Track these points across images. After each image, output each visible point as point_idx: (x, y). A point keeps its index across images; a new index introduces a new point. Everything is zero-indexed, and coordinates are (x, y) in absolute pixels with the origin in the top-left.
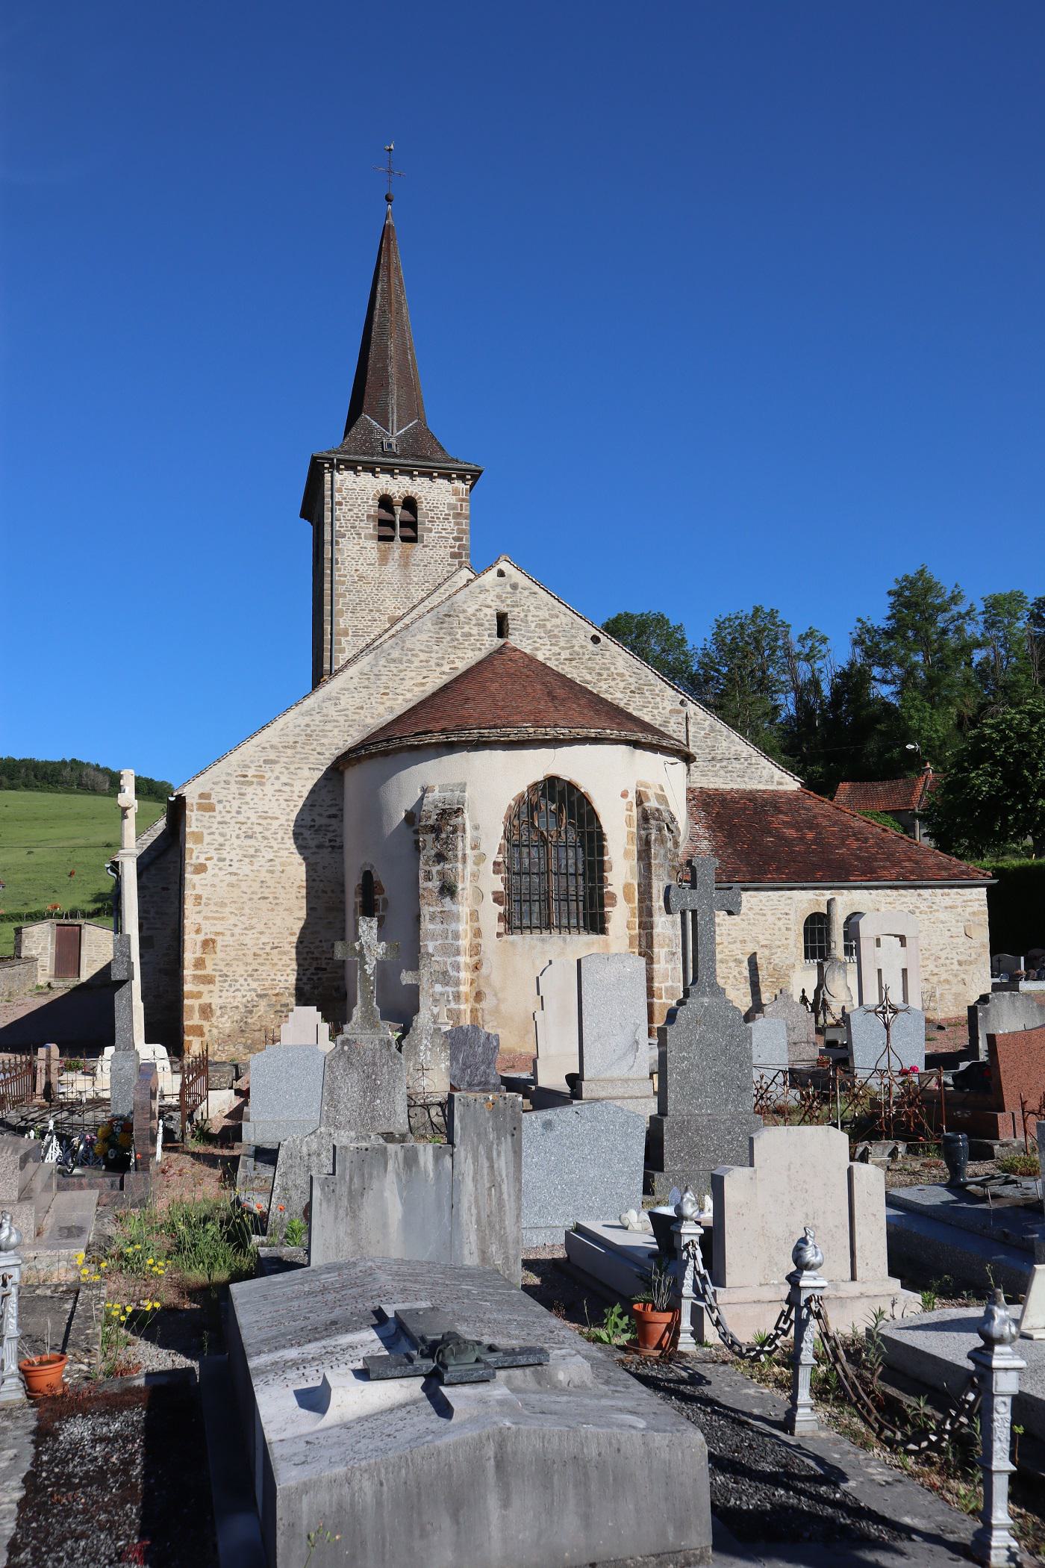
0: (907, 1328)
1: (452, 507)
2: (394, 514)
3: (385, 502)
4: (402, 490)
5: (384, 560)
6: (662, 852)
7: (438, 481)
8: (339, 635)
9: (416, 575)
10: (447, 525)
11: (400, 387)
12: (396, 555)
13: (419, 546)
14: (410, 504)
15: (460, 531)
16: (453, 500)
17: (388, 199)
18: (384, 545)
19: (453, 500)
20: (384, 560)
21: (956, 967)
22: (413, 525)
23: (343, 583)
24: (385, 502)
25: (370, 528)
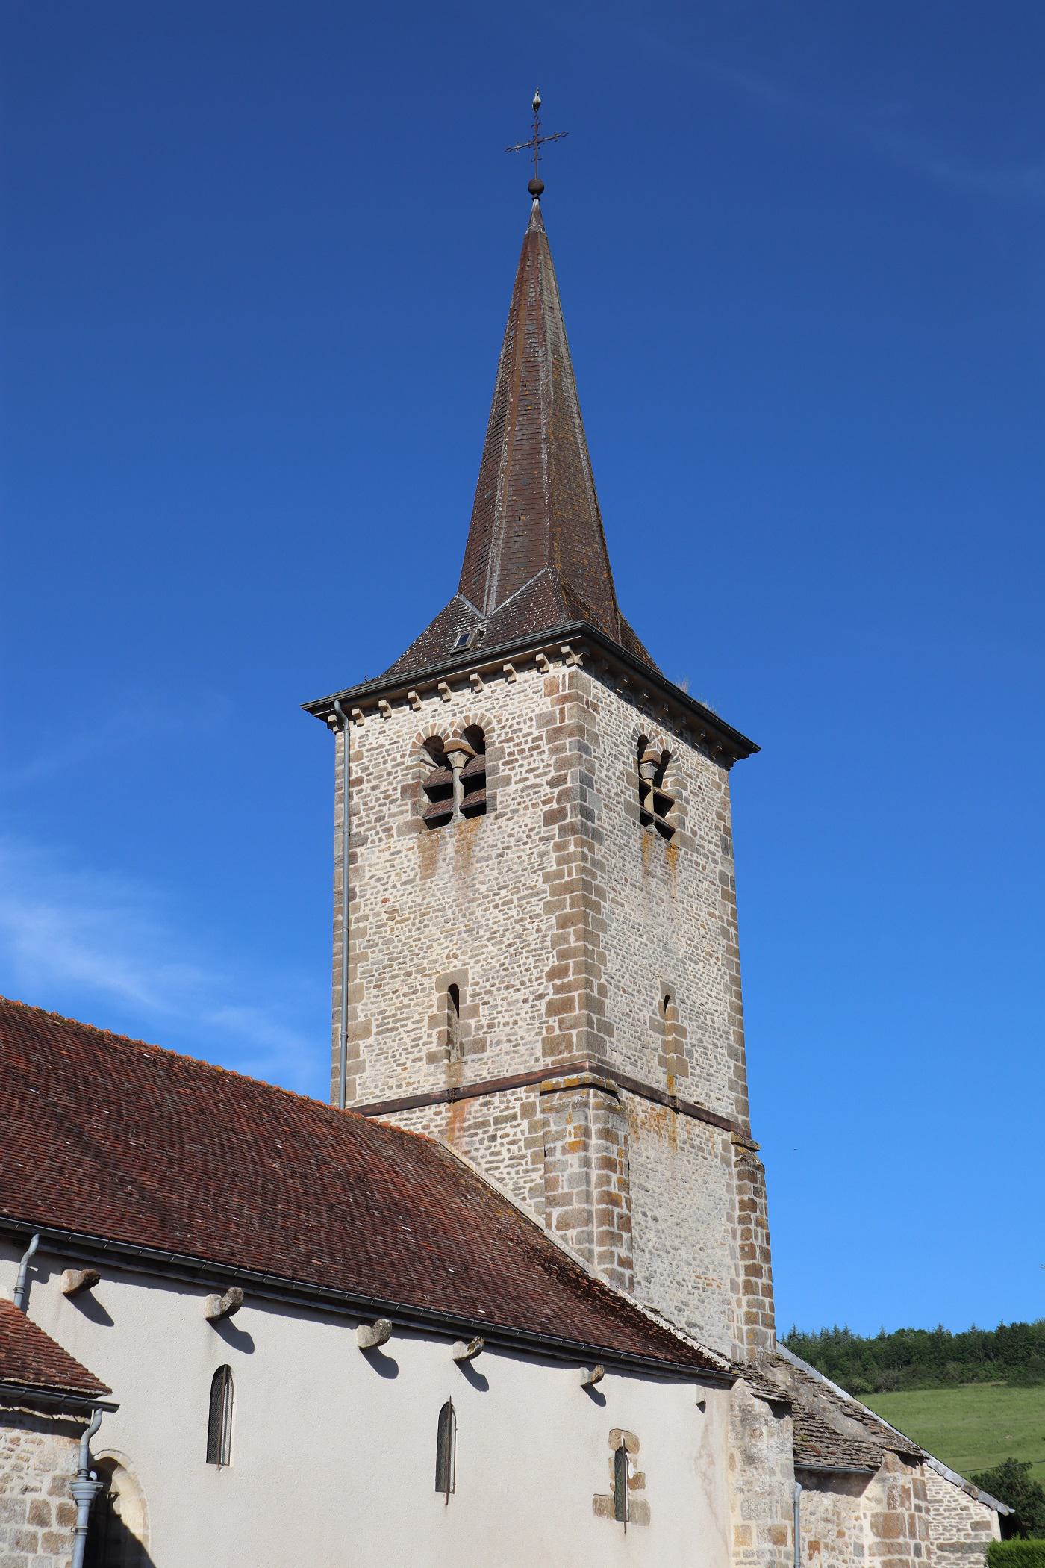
0: (713, 1513)
1: (545, 719)
2: (450, 768)
3: (435, 747)
4: (459, 719)
5: (429, 865)
8: (357, 1037)
9: (486, 875)
10: (537, 761)
12: (450, 850)
13: (488, 819)
14: (476, 736)
15: (561, 764)
17: (536, 192)
18: (429, 837)
20: (429, 865)
22: (475, 782)
23: (363, 933)
24: (435, 747)
25: (404, 813)
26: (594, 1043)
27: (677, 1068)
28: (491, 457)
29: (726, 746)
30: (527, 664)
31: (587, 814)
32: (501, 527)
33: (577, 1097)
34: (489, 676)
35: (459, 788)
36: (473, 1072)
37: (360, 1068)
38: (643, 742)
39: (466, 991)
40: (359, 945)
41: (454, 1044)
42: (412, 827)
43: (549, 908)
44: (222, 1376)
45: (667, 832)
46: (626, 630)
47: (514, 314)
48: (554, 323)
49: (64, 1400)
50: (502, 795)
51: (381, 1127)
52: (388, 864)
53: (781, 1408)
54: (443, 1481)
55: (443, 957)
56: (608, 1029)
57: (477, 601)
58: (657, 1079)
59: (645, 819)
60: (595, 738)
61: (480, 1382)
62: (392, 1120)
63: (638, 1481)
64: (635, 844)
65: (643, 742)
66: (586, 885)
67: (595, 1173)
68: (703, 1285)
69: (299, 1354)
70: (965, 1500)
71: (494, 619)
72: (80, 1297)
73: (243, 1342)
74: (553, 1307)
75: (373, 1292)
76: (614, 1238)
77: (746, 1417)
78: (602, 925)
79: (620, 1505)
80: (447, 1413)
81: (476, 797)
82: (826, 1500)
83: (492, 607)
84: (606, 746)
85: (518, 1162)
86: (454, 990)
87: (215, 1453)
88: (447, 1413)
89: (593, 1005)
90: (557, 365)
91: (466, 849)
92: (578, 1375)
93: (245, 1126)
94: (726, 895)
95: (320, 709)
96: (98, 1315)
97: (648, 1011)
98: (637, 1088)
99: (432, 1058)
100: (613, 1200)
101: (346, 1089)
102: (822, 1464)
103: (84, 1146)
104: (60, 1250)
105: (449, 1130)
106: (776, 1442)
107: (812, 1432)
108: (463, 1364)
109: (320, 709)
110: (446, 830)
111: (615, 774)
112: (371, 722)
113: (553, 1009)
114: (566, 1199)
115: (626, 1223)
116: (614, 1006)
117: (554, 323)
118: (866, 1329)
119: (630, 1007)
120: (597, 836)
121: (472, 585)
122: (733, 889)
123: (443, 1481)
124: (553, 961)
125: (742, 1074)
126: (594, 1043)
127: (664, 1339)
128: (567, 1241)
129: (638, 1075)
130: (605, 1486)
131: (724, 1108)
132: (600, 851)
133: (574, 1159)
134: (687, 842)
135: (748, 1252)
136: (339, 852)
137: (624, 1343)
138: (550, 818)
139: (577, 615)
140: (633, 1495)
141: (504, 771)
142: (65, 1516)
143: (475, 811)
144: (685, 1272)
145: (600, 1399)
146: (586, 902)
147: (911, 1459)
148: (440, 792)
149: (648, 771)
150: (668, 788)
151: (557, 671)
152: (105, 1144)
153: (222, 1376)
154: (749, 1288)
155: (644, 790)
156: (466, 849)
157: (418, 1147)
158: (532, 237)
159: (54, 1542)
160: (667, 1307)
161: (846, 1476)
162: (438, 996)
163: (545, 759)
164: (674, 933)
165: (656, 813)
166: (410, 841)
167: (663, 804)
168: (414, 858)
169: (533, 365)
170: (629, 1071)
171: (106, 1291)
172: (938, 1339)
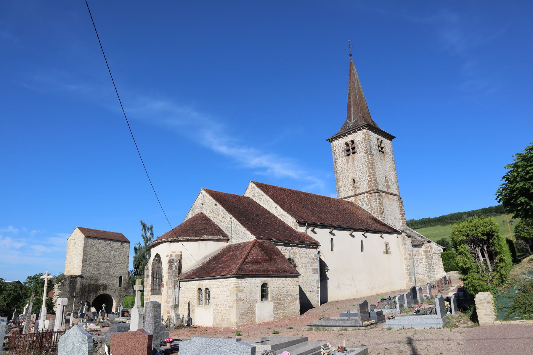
1: (363, 138)
3: (347, 144)
5: (348, 162)
6: (171, 271)
7: (353, 134)
9: (357, 163)
10: (362, 145)
11: (354, 107)
13: (356, 154)
14: (353, 142)
15: (366, 145)
16: (363, 136)
17: (351, 55)
19: (363, 136)
20: (348, 162)
21: (228, 308)
24: (347, 144)
25: (343, 154)
26: (376, 186)
27: (388, 188)
28: (349, 98)
29: (390, 137)
30: (359, 130)
31: (371, 152)
32: (352, 109)
33: (374, 194)
34: (354, 132)
35: (351, 150)
36: (358, 192)
37: (341, 192)
38: (378, 139)
39: (356, 180)
40: (339, 174)
41: (355, 188)
42: (344, 156)
43: (367, 167)
44: (332, 239)
45: (383, 152)
46: (373, 122)
47: (350, 75)
48: (356, 75)
49: (314, 245)
50: (357, 150)
51: (346, 201)
52: (341, 162)
53: (409, 237)
54: (362, 251)
55: (352, 175)
56: (378, 184)
57: (350, 121)
58: (385, 190)
59: (380, 151)
60: (371, 140)
61: (366, 237)
62: (347, 200)
63: (389, 249)
64: (379, 155)
65: (378, 139)
66: (372, 163)
67: (378, 205)
68: (395, 219)
69: (341, 235)
70: (437, 247)
71: (353, 123)
72: (313, 231)
73: (334, 235)
74: (374, 225)
75: (350, 226)
76: (382, 214)
77: (404, 238)
78: (375, 168)
79: (387, 252)
80: (362, 241)
81: (354, 151)
82: (416, 249)
83: (352, 121)
84: (373, 141)
85: (366, 204)
86: (354, 180)
87: (332, 250)
88: (362, 241)
89: (375, 180)
90: (358, 82)
91: (353, 159)
92: (379, 235)
93: (328, 204)
94: (393, 161)
95: (328, 140)
96: (315, 233)
97: (383, 180)
98: (383, 192)
99: (352, 190)
100: (381, 209)
101: (339, 196)
102: (416, 244)
103: (309, 210)
104: (310, 225)
105: (355, 200)
106: (409, 241)
107: (414, 239)
108: (363, 235)
109: (328, 140)
110: (350, 156)
111: (375, 145)
112: (336, 141)
113: (369, 181)
114: (374, 209)
115: (383, 212)
116: (378, 180)
117: (356, 75)
118: (417, 218)
119: (381, 180)
120: (373, 155)
121: (349, 118)
122: (394, 160)
123: (362, 251)
124: (368, 174)
125: (398, 187)
126: (376, 186)
127: (391, 228)
128: (375, 215)
129: (383, 190)
130: (385, 250)
131: (396, 193)
132: (374, 157)
133: (375, 203)
134: (386, 153)
135: (402, 214)
136: (334, 161)
137: (386, 229)
138: (366, 153)
139: (366, 122)
140: (388, 250)
141: (358, 147)
142: (317, 259)
143: (354, 153)
144: (393, 218)
145: (383, 238)
146: (373, 165)
147: (429, 242)
148: (348, 151)
149: (379, 144)
150: (382, 146)
151: (364, 131)
152: (311, 209)
153: (332, 239)
154: (402, 219)
155: (379, 146)
156: (353, 159)
157: (351, 203)
158: (351, 63)
159: (316, 262)
160: (390, 223)
161: (419, 245)
162: (352, 181)
163: (364, 144)
164: (386, 168)
165: (381, 150)
166: (344, 158)
167: (382, 148)
168: (345, 161)
169: (354, 83)
170: (381, 189)
171: (316, 230)
172: (429, 219)
